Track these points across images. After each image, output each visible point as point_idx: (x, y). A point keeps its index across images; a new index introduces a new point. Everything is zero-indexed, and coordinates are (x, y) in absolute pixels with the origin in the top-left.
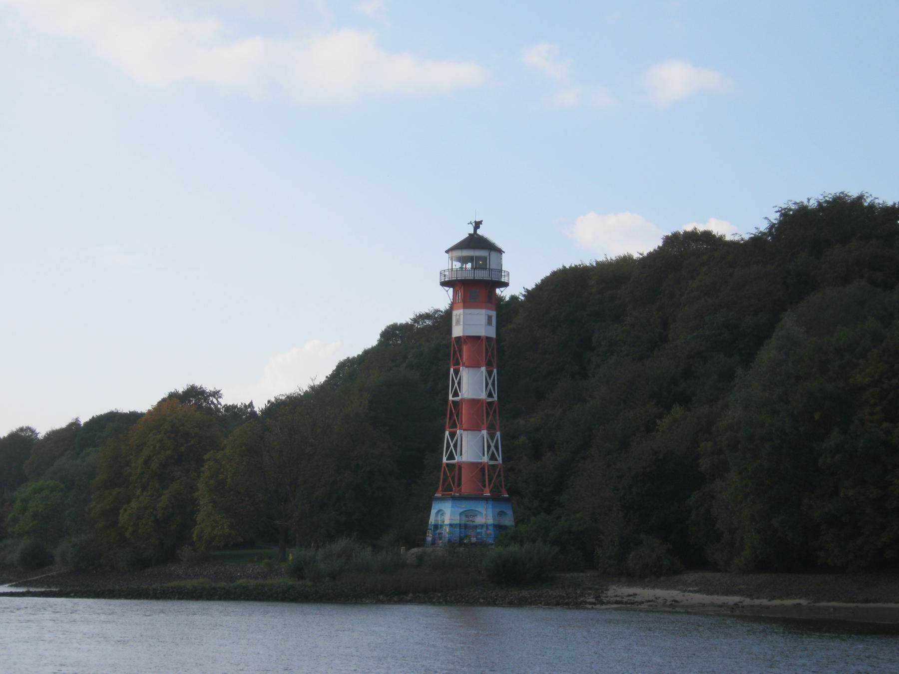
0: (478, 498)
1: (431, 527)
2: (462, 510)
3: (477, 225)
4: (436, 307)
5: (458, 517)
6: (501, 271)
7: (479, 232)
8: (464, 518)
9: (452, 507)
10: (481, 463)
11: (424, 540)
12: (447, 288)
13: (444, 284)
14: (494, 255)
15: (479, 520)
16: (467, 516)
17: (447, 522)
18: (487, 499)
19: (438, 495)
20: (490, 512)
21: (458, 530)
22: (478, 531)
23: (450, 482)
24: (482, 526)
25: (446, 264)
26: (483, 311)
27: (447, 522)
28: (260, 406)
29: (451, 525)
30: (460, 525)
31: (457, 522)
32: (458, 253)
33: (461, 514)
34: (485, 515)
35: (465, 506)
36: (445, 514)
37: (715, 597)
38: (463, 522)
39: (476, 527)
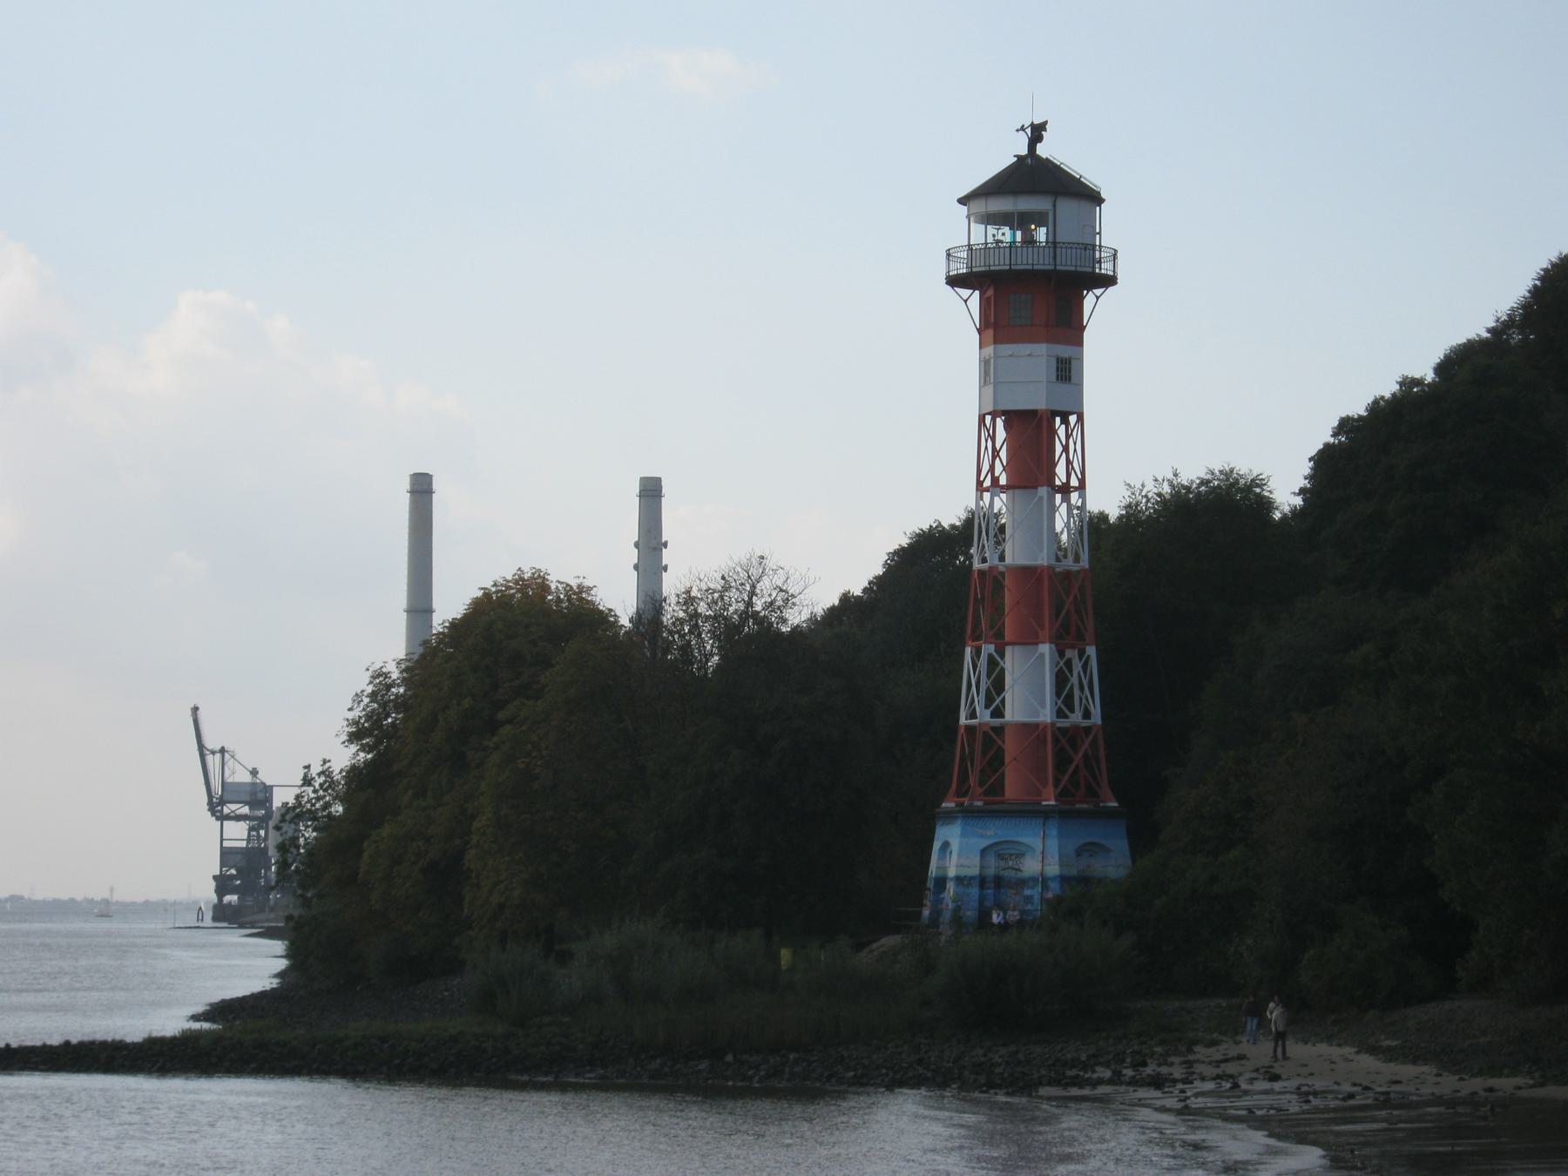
0: (1029, 812)
1: (930, 884)
2: (985, 843)
3: (1037, 133)
4: (1378, 394)
5: (977, 861)
6: (1092, 247)
7: (1042, 150)
8: (992, 861)
9: (963, 835)
10: (1037, 725)
11: (920, 913)
12: (965, 293)
13: (954, 281)
14: (1067, 209)
15: (1031, 866)
16: (1000, 857)
17: (952, 873)
18: (1109, 814)
19: (948, 805)
20: (1053, 844)
21: (974, 891)
22: (1027, 892)
23: (971, 770)
24: (1034, 879)
25: (961, 232)
26: (1042, 349)
27: (952, 873)
28: (837, 602)
29: (959, 880)
30: (982, 881)
31: (975, 871)
32: (980, 206)
33: (983, 852)
34: (1042, 855)
35: (993, 832)
36: (956, 851)
37: (1407, 1071)
38: (991, 871)
39: (1022, 883)
